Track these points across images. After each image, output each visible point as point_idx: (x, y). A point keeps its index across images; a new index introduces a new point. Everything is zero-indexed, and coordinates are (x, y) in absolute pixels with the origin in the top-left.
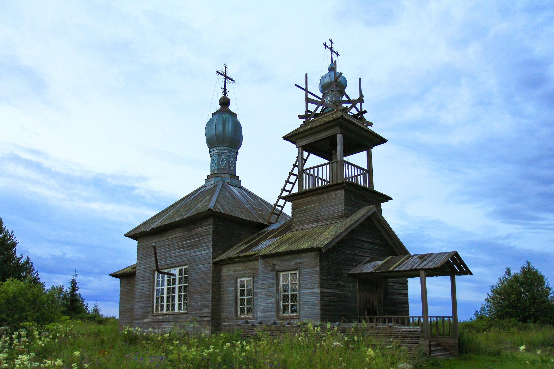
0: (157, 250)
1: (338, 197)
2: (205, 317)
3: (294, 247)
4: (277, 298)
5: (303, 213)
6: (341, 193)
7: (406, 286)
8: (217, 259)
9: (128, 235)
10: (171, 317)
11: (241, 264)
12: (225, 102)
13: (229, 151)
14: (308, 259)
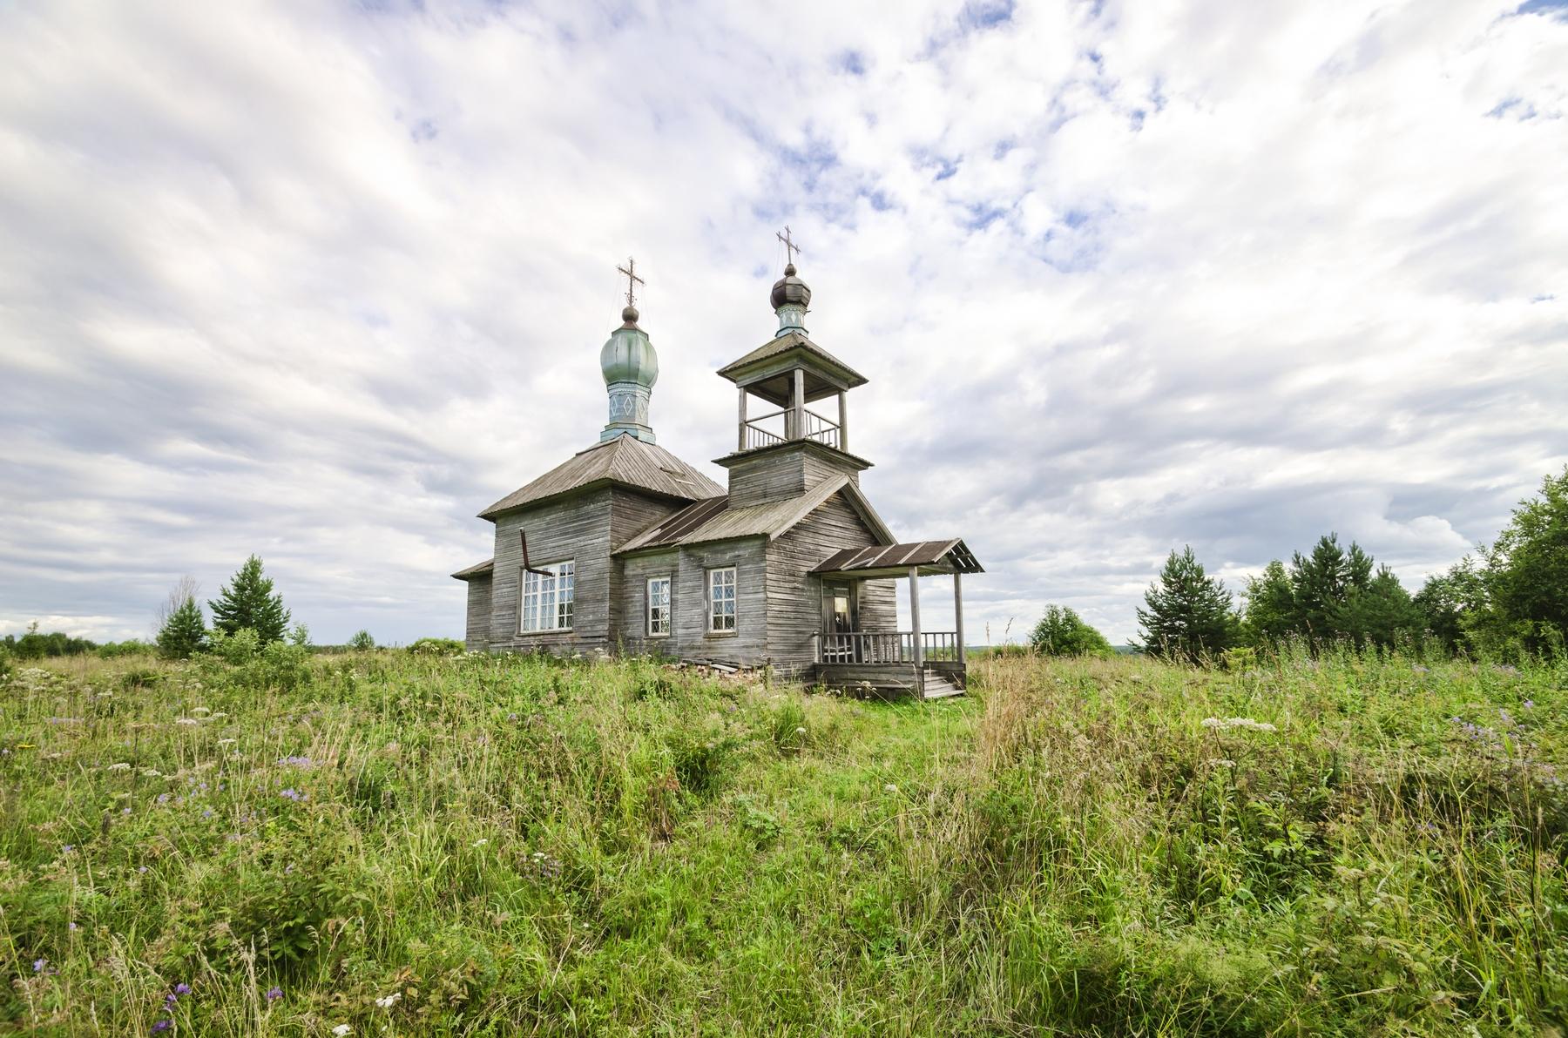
12: (630, 317)
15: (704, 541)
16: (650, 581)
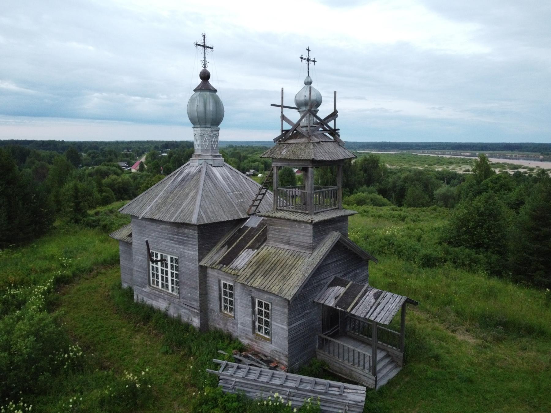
4: (254, 319)
12: (205, 76)
13: (212, 131)
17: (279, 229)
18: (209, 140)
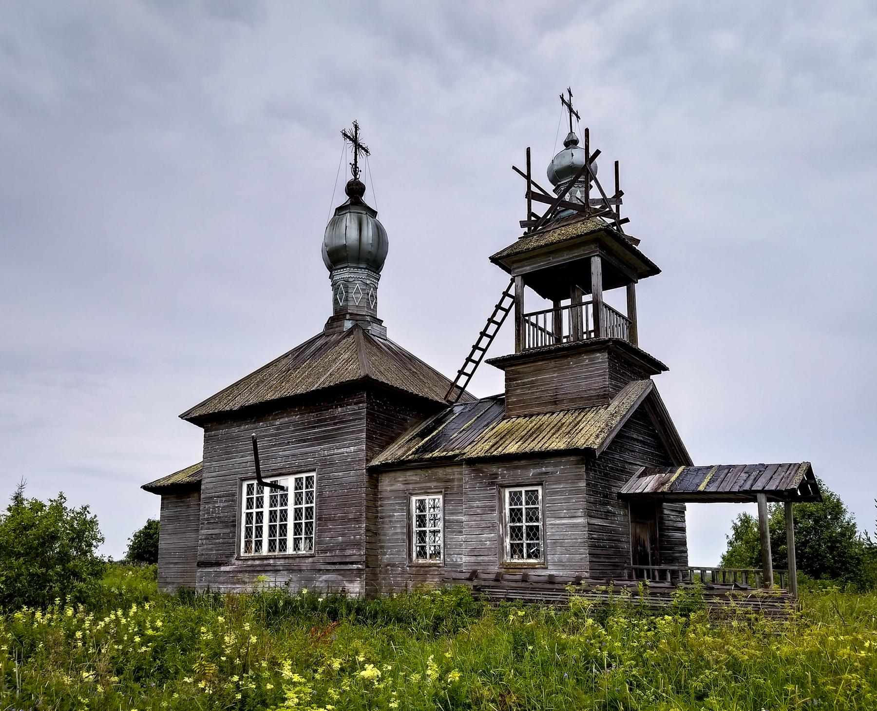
0: (258, 442)
1: (596, 363)
2: (352, 563)
3: (535, 445)
5: (527, 387)
6: (602, 358)
7: (683, 515)
8: (375, 462)
9: (188, 417)
10: (282, 562)
11: (419, 471)
12: (355, 190)
13: (368, 275)
14: (562, 467)
15: (261, 404)
16: (414, 499)
17: (532, 382)
18: (362, 290)
